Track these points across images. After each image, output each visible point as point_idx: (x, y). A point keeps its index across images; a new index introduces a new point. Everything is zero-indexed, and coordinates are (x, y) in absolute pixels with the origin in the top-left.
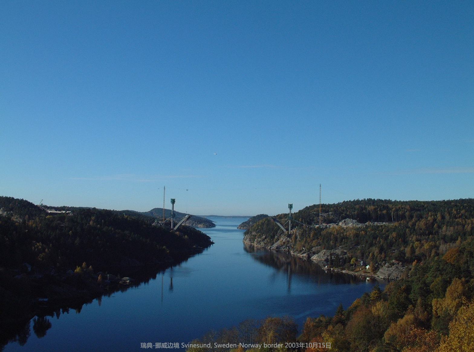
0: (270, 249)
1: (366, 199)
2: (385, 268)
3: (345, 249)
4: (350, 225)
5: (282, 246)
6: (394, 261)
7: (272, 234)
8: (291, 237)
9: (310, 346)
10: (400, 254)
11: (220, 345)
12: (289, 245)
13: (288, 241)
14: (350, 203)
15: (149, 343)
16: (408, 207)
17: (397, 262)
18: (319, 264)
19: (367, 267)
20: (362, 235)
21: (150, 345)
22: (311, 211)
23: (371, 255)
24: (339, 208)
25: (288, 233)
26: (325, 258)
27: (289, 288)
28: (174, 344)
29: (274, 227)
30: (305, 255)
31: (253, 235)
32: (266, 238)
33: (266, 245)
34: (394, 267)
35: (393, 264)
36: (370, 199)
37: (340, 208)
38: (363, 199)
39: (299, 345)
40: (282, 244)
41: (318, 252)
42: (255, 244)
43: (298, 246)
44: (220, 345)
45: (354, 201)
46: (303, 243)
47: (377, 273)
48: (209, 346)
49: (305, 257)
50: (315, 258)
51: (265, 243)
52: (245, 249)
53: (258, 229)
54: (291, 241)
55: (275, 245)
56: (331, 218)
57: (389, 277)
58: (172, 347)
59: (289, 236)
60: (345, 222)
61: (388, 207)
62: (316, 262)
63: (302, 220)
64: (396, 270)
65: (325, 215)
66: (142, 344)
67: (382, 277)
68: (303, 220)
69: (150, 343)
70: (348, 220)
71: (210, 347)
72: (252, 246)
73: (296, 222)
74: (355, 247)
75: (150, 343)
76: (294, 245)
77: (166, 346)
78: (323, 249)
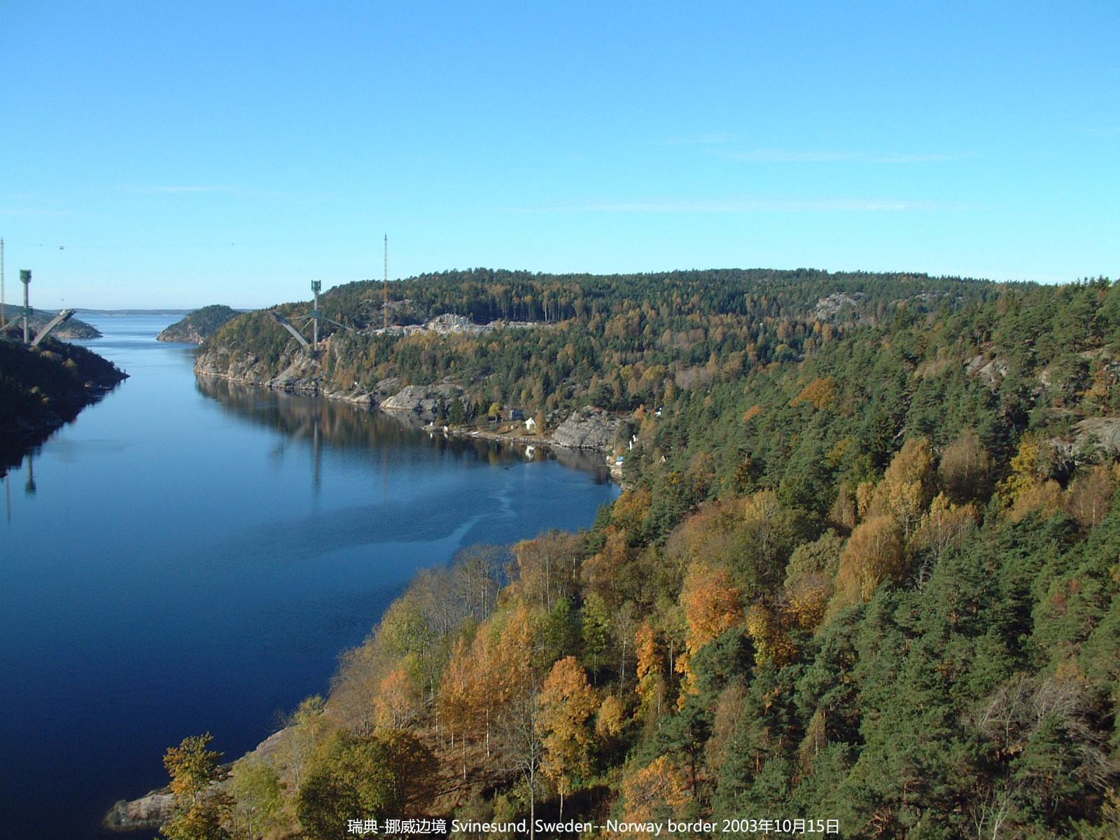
0: (270, 386)
1: (473, 270)
2: (570, 424)
3: (459, 384)
4: (455, 328)
5: (299, 379)
6: (589, 407)
7: (271, 352)
8: (320, 358)
9: (787, 828)
10: (603, 393)
11: (550, 825)
12: (315, 376)
13: (314, 368)
14: (437, 278)
15: (369, 821)
16: (577, 288)
17: (597, 410)
18: (400, 418)
19: (529, 422)
20: (494, 351)
21: (372, 825)
22: (361, 297)
23: (523, 394)
24: (424, 290)
25: (312, 348)
26: (414, 404)
27: (317, 481)
28: (434, 823)
29: (276, 335)
30: (363, 398)
31: (222, 355)
32: (256, 361)
33: (259, 378)
34: (591, 422)
35: (589, 415)
36: (482, 268)
37: (427, 289)
38: (465, 269)
39: (758, 827)
40: (299, 373)
41: (393, 392)
42: (230, 376)
43: (339, 377)
44: (550, 825)
45: (445, 274)
46: (352, 372)
47: (553, 436)
48: (521, 827)
49: (365, 403)
50: (389, 405)
51: (255, 373)
52: (202, 389)
53: (231, 340)
54: (319, 366)
55: (283, 378)
56: (409, 312)
57: (582, 442)
58: (427, 831)
59: (316, 355)
60: (441, 321)
61: (532, 288)
62: (392, 414)
63: (342, 318)
64: (597, 427)
65: (396, 306)
66: (352, 823)
67: (565, 443)
68: (346, 317)
69: (372, 821)
70: (447, 317)
71: (524, 830)
72: (220, 381)
73: (330, 323)
74: (482, 378)
75: (372, 821)
76: (329, 377)
77: (412, 829)
78: (405, 383)
